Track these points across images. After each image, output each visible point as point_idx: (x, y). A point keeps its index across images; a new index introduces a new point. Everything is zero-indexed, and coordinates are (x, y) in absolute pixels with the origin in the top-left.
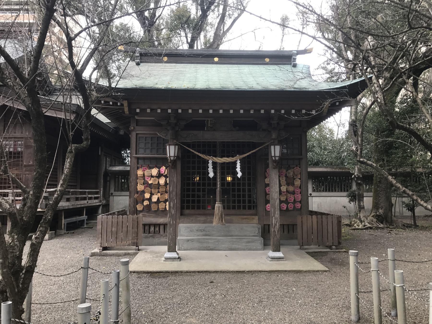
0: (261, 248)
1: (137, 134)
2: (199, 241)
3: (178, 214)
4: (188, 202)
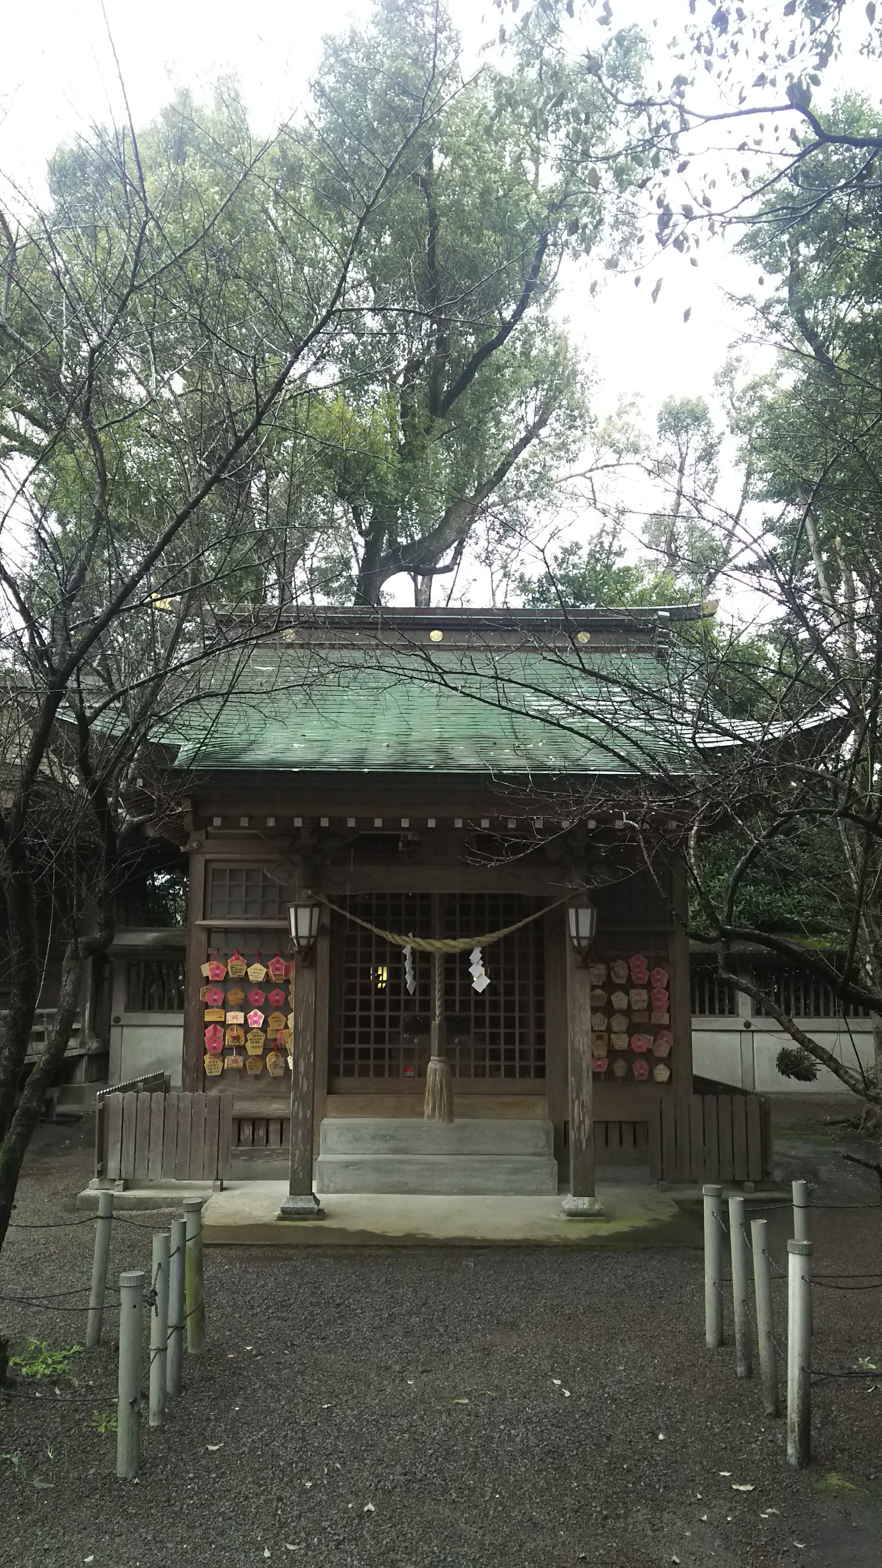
0: (550, 1187)
1: (207, 862)
2: (377, 1167)
3: (321, 1092)
4: (350, 1053)
